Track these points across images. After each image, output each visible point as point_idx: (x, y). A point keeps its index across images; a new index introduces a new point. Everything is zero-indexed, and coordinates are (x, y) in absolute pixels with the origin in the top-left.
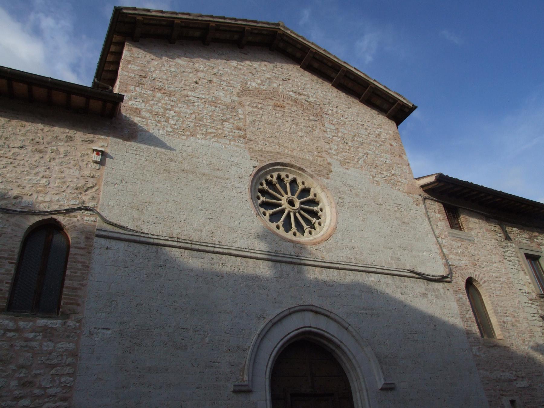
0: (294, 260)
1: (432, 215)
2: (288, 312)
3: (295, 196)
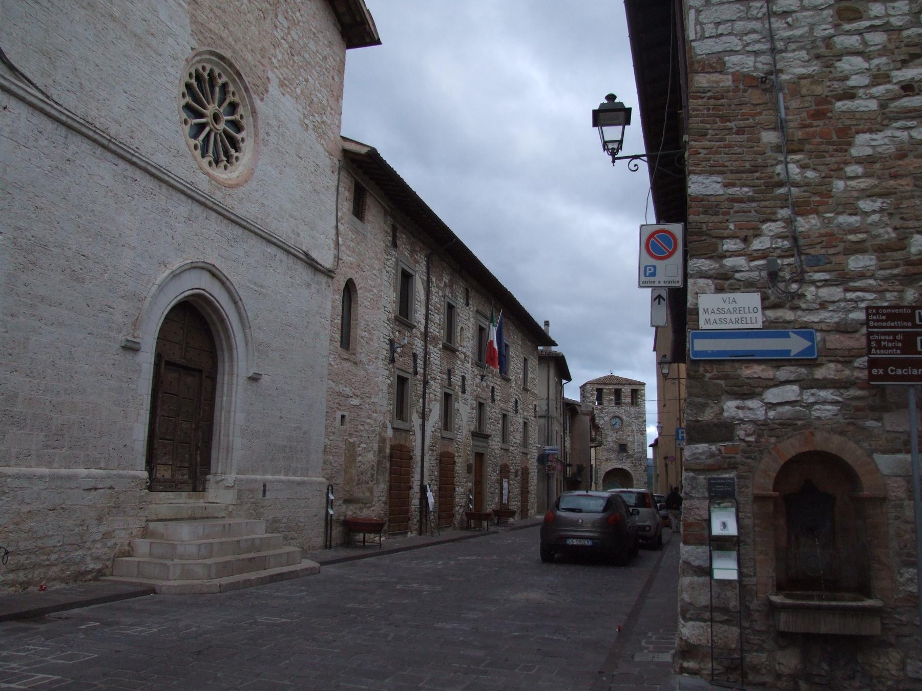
0: (207, 202)
1: (341, 189)
2: (189, 266)
3: (221, 110)
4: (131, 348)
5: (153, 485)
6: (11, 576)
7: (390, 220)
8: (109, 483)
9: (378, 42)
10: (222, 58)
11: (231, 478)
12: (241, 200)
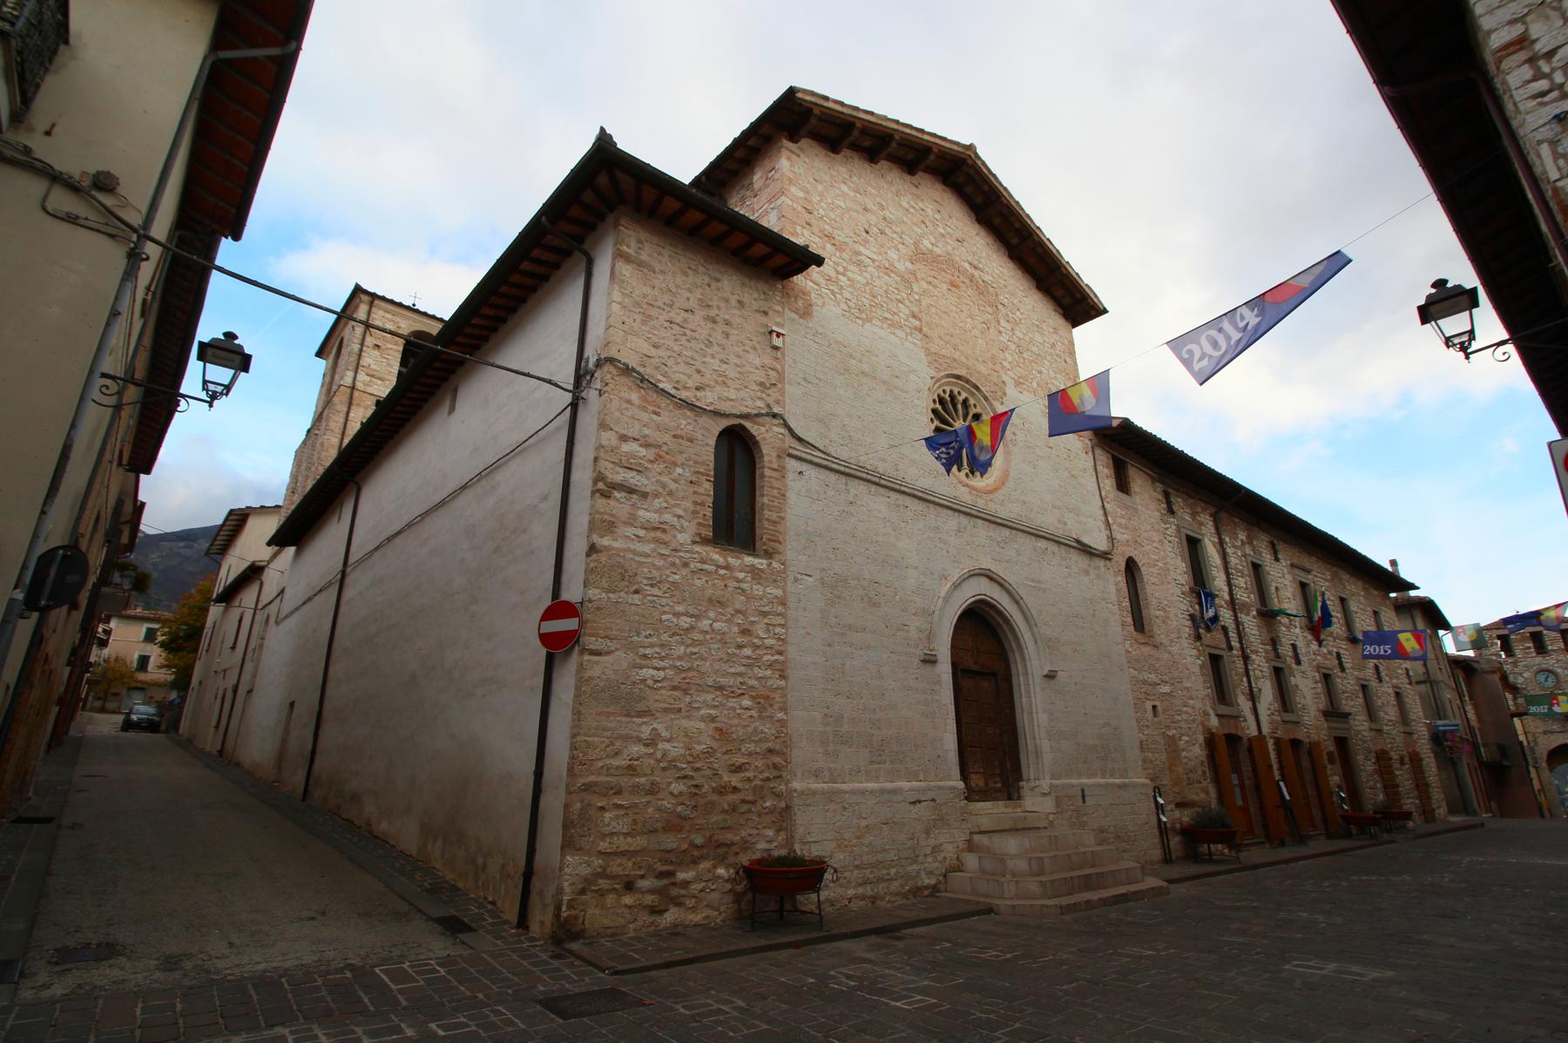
4: (929, 661)
5: (971, 794)
6: (860, 890)
7: (1160, 487)
8: (930, 795)
9: (1105, 311)
10: (958, 377)
11: (1045, 784)
12: (1002, 503)
